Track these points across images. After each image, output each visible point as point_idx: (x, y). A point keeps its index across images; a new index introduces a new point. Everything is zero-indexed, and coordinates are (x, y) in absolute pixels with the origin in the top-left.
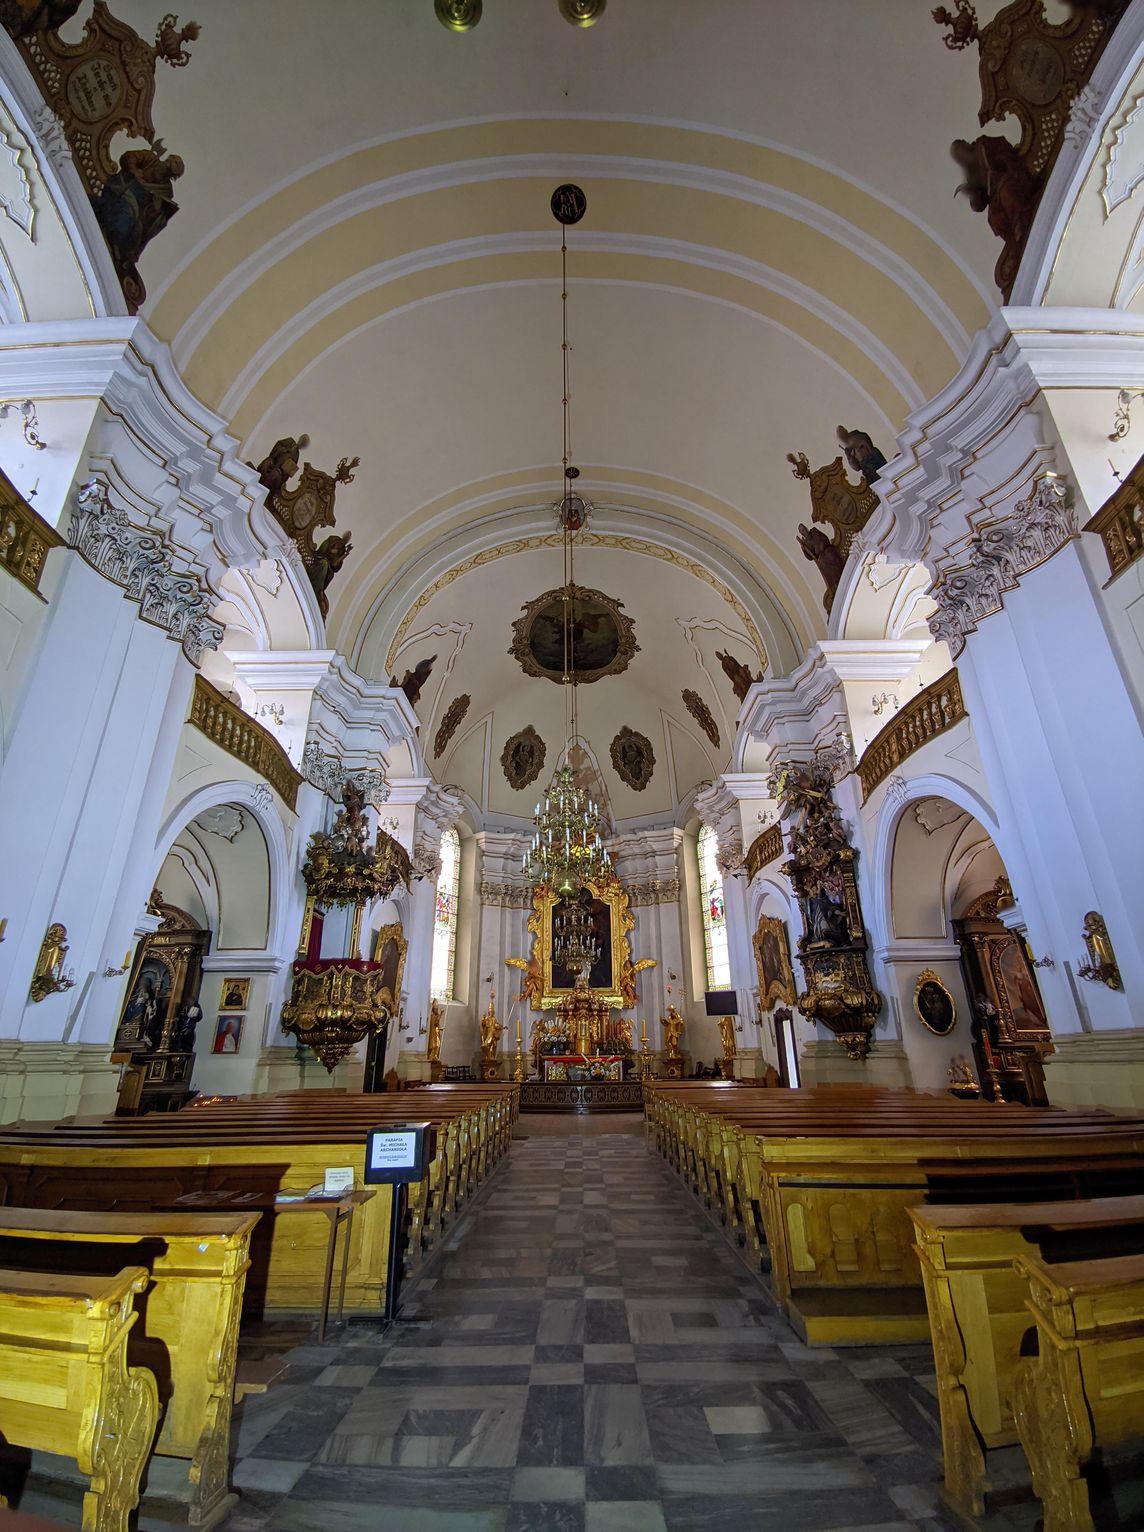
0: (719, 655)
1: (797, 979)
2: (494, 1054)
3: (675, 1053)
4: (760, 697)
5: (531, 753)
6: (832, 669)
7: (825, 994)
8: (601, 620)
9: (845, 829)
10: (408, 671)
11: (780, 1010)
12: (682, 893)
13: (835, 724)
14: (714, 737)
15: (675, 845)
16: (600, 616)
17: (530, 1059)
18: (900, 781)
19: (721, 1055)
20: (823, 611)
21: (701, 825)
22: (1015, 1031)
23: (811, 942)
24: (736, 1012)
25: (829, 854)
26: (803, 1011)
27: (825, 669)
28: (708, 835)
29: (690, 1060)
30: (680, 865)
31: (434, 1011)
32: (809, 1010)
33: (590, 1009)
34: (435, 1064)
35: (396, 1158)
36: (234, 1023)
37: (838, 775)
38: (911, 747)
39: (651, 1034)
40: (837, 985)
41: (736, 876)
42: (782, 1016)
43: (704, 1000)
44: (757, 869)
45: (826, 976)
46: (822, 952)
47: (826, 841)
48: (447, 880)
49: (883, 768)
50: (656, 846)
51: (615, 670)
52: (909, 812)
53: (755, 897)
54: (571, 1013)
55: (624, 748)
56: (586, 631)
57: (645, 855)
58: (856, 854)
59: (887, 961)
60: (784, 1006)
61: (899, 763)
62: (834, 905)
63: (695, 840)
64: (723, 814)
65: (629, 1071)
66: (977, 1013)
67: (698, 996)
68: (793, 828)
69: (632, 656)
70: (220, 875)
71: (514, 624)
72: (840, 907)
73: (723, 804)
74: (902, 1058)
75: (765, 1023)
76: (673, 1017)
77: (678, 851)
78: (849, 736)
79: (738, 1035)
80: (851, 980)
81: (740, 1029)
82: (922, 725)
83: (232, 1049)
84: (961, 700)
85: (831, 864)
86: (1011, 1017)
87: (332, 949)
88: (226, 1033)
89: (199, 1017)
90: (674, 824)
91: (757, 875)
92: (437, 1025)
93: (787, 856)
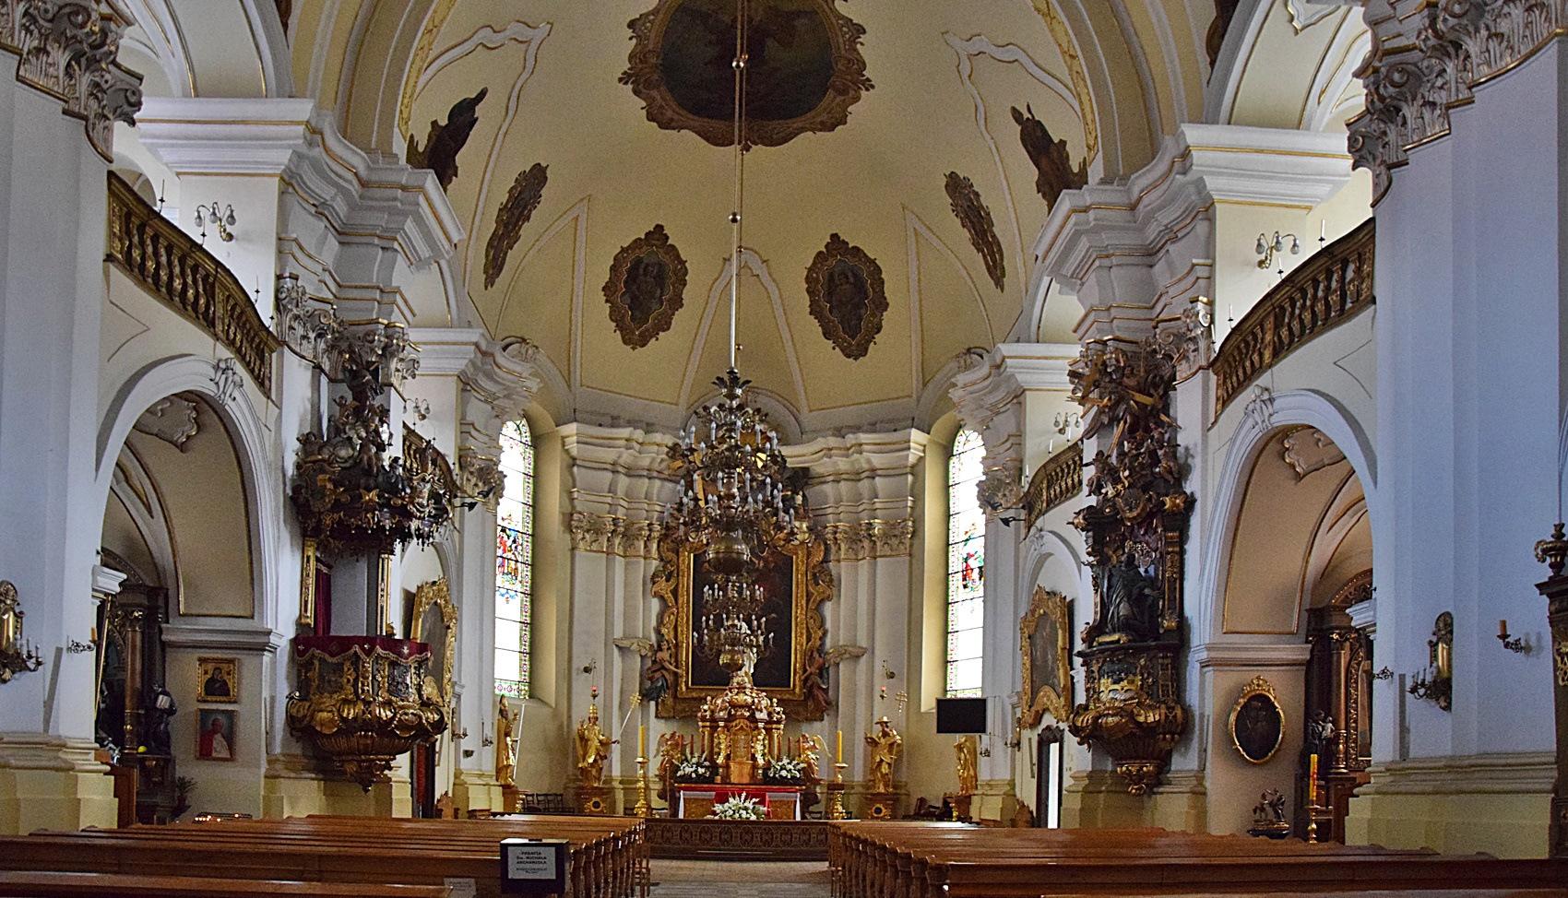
0: (1017, 115)
1: (1077, 686)
2: (599, 780)
3: (886, 786)
4: (1073, 219)
5: (660, 280)
6: (1201, 179)
7: (1108, 709)
8: (800, 23)
9: (1181, 461)
10: (434, 123)
11: (1048, 728)
12: (916, 542)
13: (1191, 279)
14: (996, 271)
15: (912, 459)
16: (798, 14)
17: (656, 787)
18: (1266, 396)
19: (955, 788)
20: (1204, 58)
21: (959, 427)
22: (1356, 759)
23: (1103, 633)
24: (983, 729)
25: (1150, 499)
26: (1075, 730)
27: (1189, 177)
28: (968, 446)
29: (908, 795)
30: (918, 494)
31: (502, 712)
32: (1083, 729)
33: (753, 719)
34: (508, 791)
35: (534, 870)
36: (222, 719)
37: (1183, 370)
38: (1291, 342)
39: (849, 756)
40: (1128, 695)
41: (1006, 522)
42: (1052, 736)
43: (934, 711)
44: (1042, 513)
45: (1115, 683)
46: (1114, 649)
47: (1150, 478)
48: (513, 507)
49: (1249, 370)
50: (878, 460)
51: (822, 123)
52: (1273, 446)
53: (1033, 555)
54: (722, 724)
55: (831, 275)
56: (770, 42)
57: (856, 476)
58: (1190, 502)
59: (1204, 665)
60: (1053, 723)
61: (1270, 366)
62: (1144, 579)
63: (947, 452)
64: (998, 413)
65: (811, 808)
66: (1310, 741)
67: (928, 702)
68: (1100, 453)
69: (857, 99)
70: (170, 501)
71: (631, 25)
72: (1152, 582)
73: (1000, 394)
74: (1199, 793)
75: (1025, 744)
76: (885, 734)
77: (917, 470)
78: (1211, 304)
79: (982, 760)
80: (1149, 694)
81: (987, 753)
82: (1326, 298)
83: (225, 754)
84: (1371, 275)
85: (1151, 515)
86: (1355, 741)
87: (348, 622)
88: (215, 732)
89: (171, 711)
90: (914, 423)
91: (1039, 523)
92: (507, 734)
93: (1085, 500)
